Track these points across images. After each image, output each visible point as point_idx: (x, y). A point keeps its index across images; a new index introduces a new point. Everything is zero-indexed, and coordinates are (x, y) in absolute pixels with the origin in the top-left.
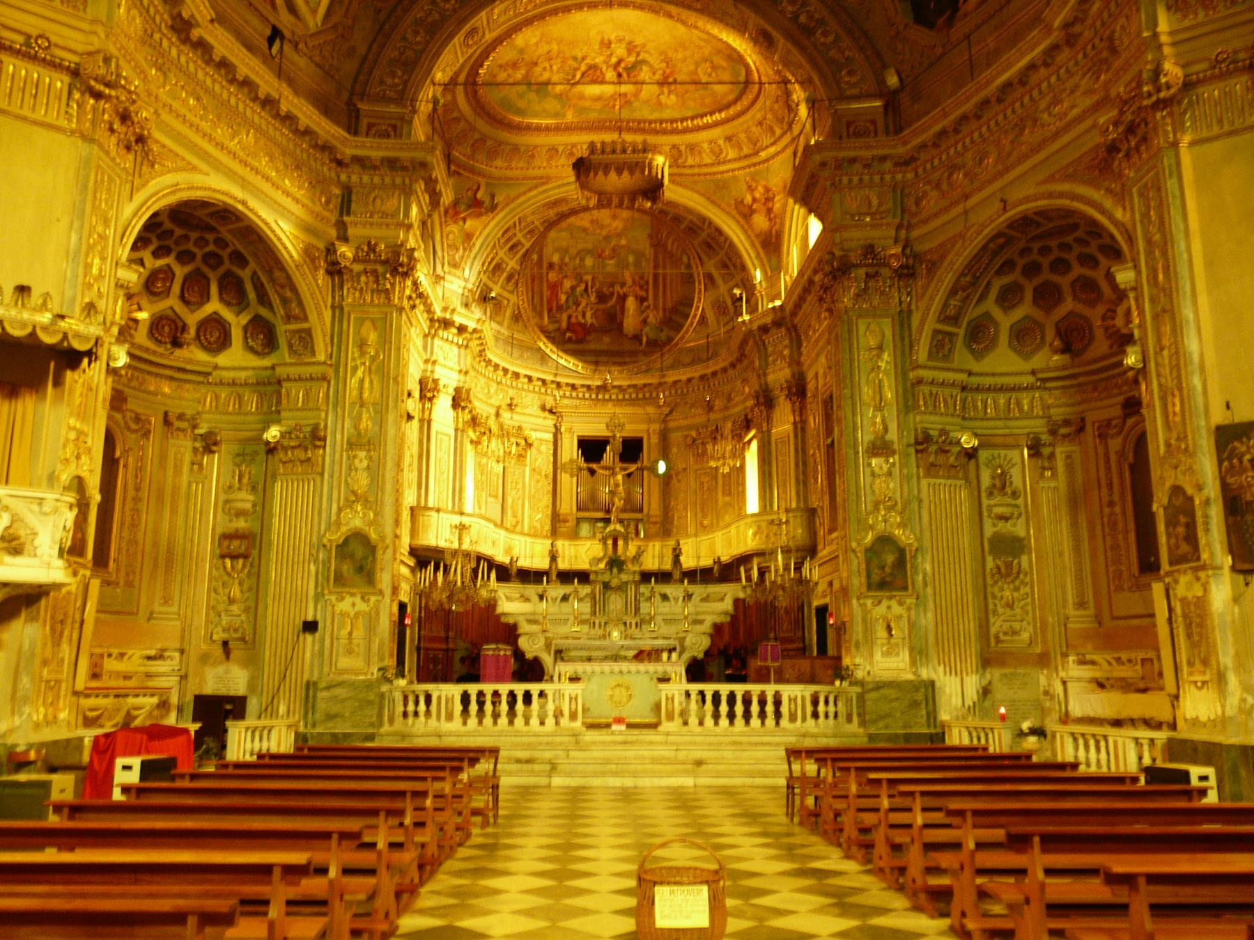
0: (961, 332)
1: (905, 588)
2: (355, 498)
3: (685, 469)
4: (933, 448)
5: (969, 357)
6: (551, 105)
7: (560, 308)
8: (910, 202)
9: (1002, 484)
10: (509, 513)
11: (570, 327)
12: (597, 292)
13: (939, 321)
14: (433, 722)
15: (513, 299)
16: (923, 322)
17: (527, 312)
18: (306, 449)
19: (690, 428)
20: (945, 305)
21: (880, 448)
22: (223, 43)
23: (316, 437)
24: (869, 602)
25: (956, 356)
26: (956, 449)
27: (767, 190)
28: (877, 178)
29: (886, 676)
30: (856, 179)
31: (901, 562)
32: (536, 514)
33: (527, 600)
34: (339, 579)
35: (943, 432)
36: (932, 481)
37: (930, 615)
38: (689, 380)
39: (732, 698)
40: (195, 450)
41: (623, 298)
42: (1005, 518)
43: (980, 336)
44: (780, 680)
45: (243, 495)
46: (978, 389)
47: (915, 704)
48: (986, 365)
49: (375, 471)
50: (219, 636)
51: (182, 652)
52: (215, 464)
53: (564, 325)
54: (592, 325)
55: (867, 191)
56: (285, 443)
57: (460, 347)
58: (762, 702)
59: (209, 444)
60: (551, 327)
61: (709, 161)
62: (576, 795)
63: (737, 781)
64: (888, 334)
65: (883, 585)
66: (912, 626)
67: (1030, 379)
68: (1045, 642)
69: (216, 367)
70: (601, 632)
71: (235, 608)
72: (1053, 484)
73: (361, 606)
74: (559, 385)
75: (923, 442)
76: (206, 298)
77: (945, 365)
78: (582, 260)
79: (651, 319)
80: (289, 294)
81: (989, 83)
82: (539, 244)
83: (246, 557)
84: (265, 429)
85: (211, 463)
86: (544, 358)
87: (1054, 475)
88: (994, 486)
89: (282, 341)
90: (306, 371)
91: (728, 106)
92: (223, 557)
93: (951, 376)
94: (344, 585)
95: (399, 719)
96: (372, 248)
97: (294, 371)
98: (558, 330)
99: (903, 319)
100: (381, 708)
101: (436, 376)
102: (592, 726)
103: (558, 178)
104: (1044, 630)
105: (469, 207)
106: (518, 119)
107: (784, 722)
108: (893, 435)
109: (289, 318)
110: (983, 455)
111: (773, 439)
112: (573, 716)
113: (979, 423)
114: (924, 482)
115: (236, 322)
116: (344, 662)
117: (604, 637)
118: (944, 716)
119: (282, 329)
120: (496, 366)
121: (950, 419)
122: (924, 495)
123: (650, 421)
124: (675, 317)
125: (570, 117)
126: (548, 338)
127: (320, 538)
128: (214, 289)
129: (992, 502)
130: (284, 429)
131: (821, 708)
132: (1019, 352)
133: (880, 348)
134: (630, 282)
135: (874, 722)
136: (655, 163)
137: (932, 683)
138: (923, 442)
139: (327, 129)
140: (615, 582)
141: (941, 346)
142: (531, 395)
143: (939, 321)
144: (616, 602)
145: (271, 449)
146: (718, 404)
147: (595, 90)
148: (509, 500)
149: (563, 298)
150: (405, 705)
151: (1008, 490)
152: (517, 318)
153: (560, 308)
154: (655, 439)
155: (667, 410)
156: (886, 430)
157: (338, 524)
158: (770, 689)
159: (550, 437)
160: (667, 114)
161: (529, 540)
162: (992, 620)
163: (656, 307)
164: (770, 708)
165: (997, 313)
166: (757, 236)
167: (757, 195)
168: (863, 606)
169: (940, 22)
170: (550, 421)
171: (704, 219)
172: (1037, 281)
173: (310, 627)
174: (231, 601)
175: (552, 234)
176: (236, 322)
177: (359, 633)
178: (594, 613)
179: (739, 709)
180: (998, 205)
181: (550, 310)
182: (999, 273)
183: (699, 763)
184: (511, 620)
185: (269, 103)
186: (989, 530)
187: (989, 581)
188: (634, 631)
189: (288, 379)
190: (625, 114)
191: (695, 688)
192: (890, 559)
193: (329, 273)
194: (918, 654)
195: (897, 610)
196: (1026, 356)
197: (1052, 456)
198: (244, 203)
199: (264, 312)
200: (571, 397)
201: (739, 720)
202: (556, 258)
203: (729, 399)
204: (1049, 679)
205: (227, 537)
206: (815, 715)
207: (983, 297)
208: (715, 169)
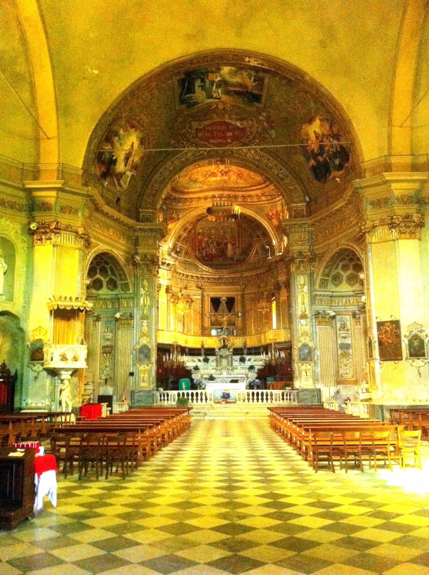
0: (330, 279)
1: (311, 360)
2: (143, 335)
3: (251, 309)
4: (320, 316)
5: (333, 286)
6: (198, 185)
7: (203, 249)
8: (314, 237)
9: (343, 327)
10: (186, 327)
11: (207, 255)
12: (217, 242)
13: (322, 276)
14: (169, 402)
15: (185, 247)
16: (317, 275)
17: (190, 250)
18: (128, 320)
19: (252, 293)
20: (324, 271)
21: (304, 316)
22: (106, 209)
23: (131, 316)
24: (300, 365)
25: (329, 287)
26: (328, 316)
27: (277, 211)
28: (303, 230)
29: (305, 387)
30: (296, 230)
31: (310, 353)
32: (195, 327)
33: (195, 361)
34: (140, 360)
35: (324, 311)
36: (320, 326)
37: (319, 369)
38: (252, 276)
39: (258, 394)
40: (94, 321)
41: (226, 244)
42: (345, 338)
43: (337, 279)
44: (273, 389)
45: (108, 334)
46: (336, 296)
47: (314, 396)
48: (338, 289)
49: (149, 326)
50: (103, 377)
51: (93, 382)
52: (99, 324)
53: (204, 255)
54: (215, 254)
55: (300, 233)
56: (122, 318)
57: (167, 270)
58: (267, 395)
59: (98, 319)
60: (199, 256)
61: (255, 200)
62: (212, 422)
63: (258, 418)
64: (306, 280)
65: (304, 359)
66: (314, 372)
67: (352, 293)
68: (356, 376)
69: (99, 294)
70: (220, 372)
71: (108, 369)
72: (359, 327)
73: (147, 368)
74: (203, 278)
75: (317, 314)
76: (96, 274)
77: (325, 290)
78: (211, 231)
79: (237, 251)
80: (121, 272)
81: (332, 208)
82: (194, 227)
83: (110, 353)
84: (115, 314)
85: (98, 324)
86: (197, 267)
87: (360, 324)
88: (341, 327)
89: (119, 286)
90: (127, 296)
91: (261, 184)
92: (103, 353)
93: (327, 293)
94: (141, 361)
95: (159, 402)
96: (146, 256)
97: (124, 296)
98: (202, 256)
99: (311, 275)
100: (153, 398)
101: (160, 282)
102: (216, 403)
103: (202, 207)
104: (356, 373)
105: (170, 220)
106: (186, 190)
107: (274, 401)
108: (307, 312)
109: (121, 280)
110: (338, 317)
111: (281, 301)
112: (211, 400)
113: (335, 308)
114: (317, 327)
115: (104, 281)
116: (142, 384)
117: (221, 374)
118: (323, 400)
119: (119, 283)
120: (180, 273)
121: (325, 307)
122: (317, 331)
123: (237, 291)
124: (246, 252)
125: (205, 187)
126: (198, 260)
127: (134, 347)
128: (98, 271)
129: (341, 332)
130: (121, 314)
131: (285, 397)
132: (350, 284)
133: (304, 285)
134: (229, 238)
135: (301, 401)
136: (235, 209)
137: (319, 390)
138: (317, 314)
139: (131, 222)
140: (224, 355)
141: (324, 284)
142: (192, 282)
143: (322, 276)
144: (224, 362)
145: (117, 320)
146: (262, 285)
147: (214, 179)
148: (186, 322)
149: (204, 245)
150: (161, 397)
151: (346, 329)
152: (187, 253)
153: (203, 249)
154: (239, 298)
155: (244, 286)
156: (305, 311)
157: (139, 342)
158: (269, 391)
159: (200, 297)
160: (240, 186)
161: (193, 337)
162: (340, 370)
163: (239, 247)
164: (269, 397)
165: (342, 272)
166: (274, 227)
167: (273, 212)
168: (298, 365)
169: (322, 181)
170: (200, 292)
171: (255, 219)
172: (353, 263)
173: (132, 374)
174: (106, 367)
175: (199, 223)
176: (104, 281)
177: (146, 376)
178: (217, 366)
179: (260, 397)
180: (336, 245)
181: (199, 249)
182: (341, 261)
183: (247, 413)
184: (189, 368)
185: (117, 220)
186: (339, 342)
187: (339, 358)
188: (232, 372)
189: (122, 298)
190: (225, 185)
191: (251, 391)
192: (306, 351)
193: (133, 265)
194: (315, 380)
195: (309, 367)
196: (352, 285)
197: (359, 317)
198: (111, 250)
199: (113, 277)
200: (208, 282)
201: (260, 401)
202: (201, 231)
203: (267, 284)
204: (358, 388)
205: (104, 347)
206: (283, 399)
207: (337, 268)
208: (258, 203)
